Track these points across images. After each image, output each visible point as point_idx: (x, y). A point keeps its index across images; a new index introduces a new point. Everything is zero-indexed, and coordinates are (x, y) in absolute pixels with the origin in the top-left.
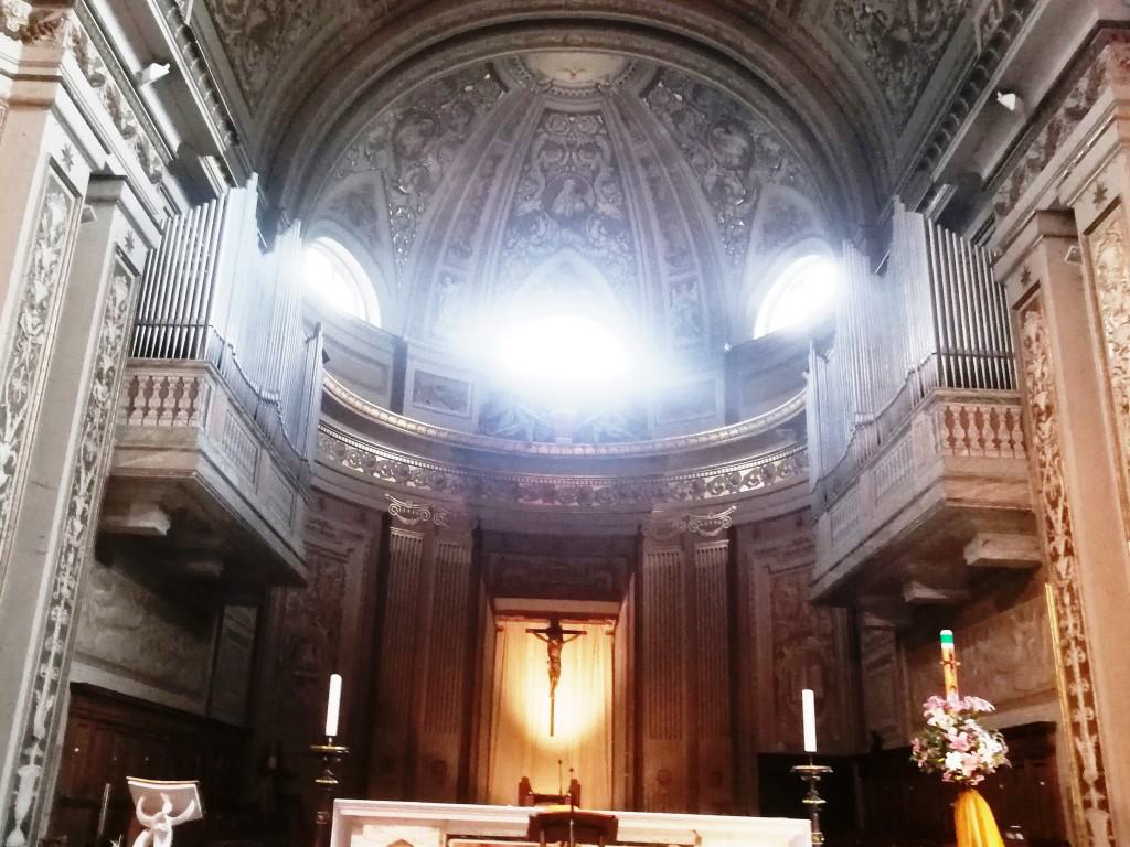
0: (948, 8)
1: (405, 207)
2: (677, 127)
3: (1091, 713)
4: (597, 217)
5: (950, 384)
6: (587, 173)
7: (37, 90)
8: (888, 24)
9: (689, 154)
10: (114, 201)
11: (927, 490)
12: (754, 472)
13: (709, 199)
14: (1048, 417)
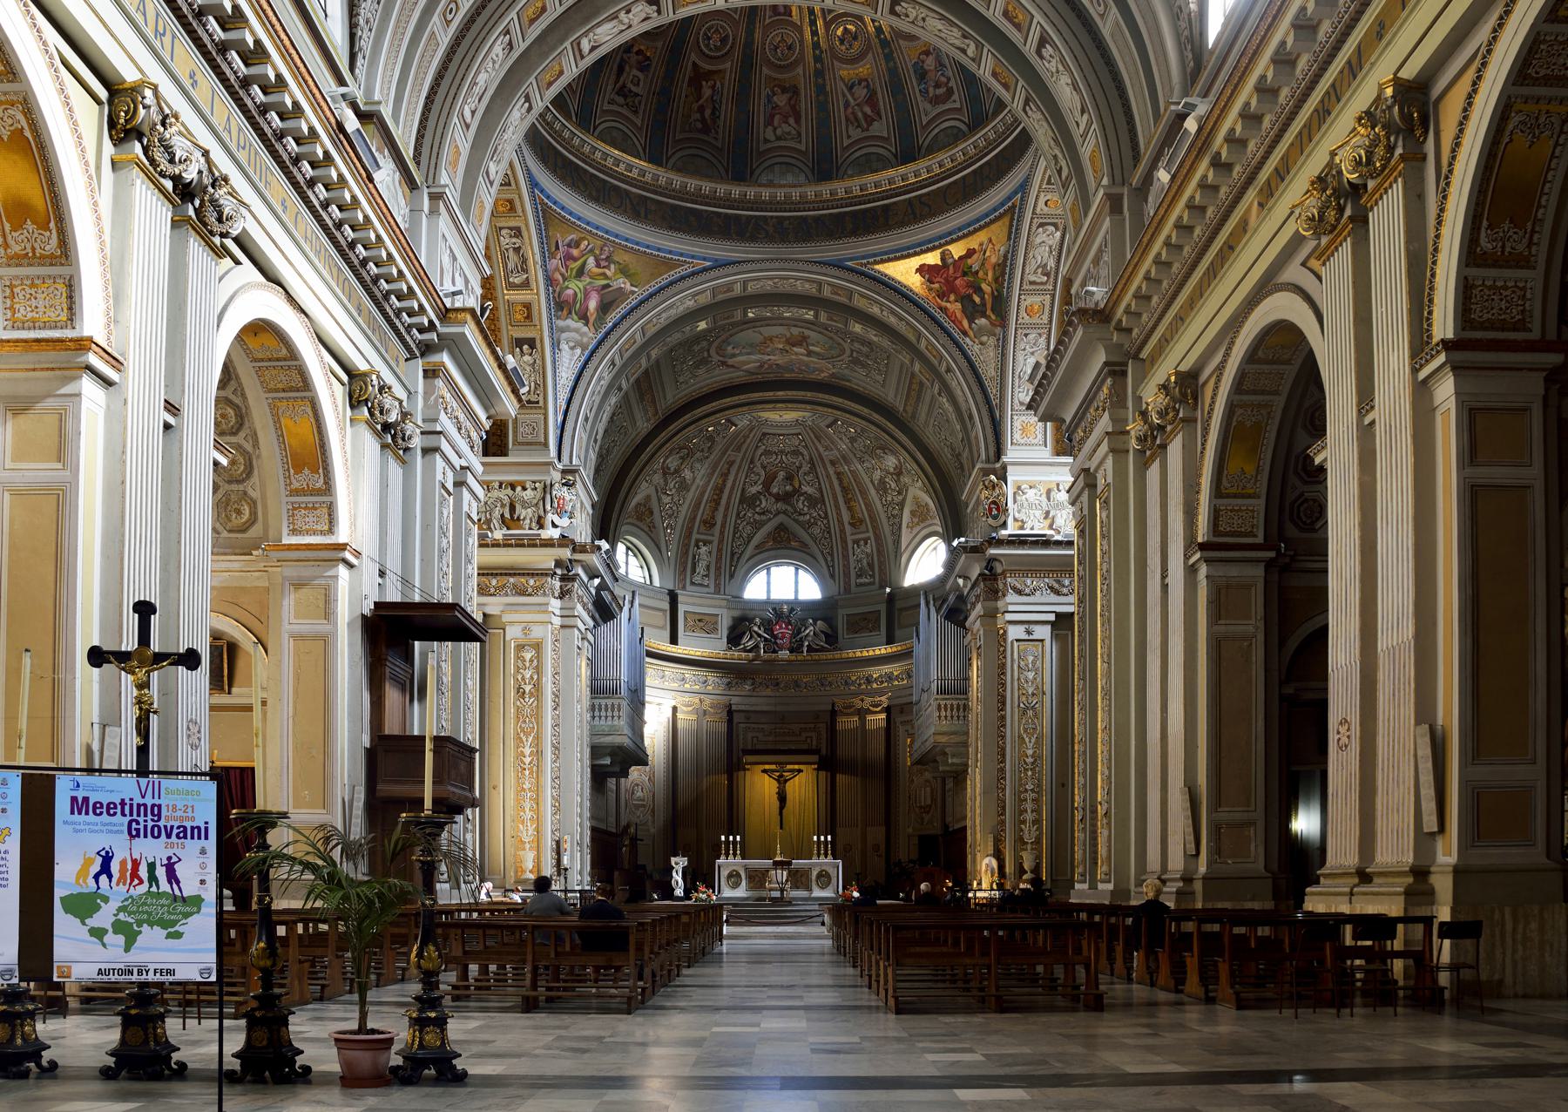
4: (802, 494)
7: (569, 621)
9: (861, 461)
10: (436, 449)
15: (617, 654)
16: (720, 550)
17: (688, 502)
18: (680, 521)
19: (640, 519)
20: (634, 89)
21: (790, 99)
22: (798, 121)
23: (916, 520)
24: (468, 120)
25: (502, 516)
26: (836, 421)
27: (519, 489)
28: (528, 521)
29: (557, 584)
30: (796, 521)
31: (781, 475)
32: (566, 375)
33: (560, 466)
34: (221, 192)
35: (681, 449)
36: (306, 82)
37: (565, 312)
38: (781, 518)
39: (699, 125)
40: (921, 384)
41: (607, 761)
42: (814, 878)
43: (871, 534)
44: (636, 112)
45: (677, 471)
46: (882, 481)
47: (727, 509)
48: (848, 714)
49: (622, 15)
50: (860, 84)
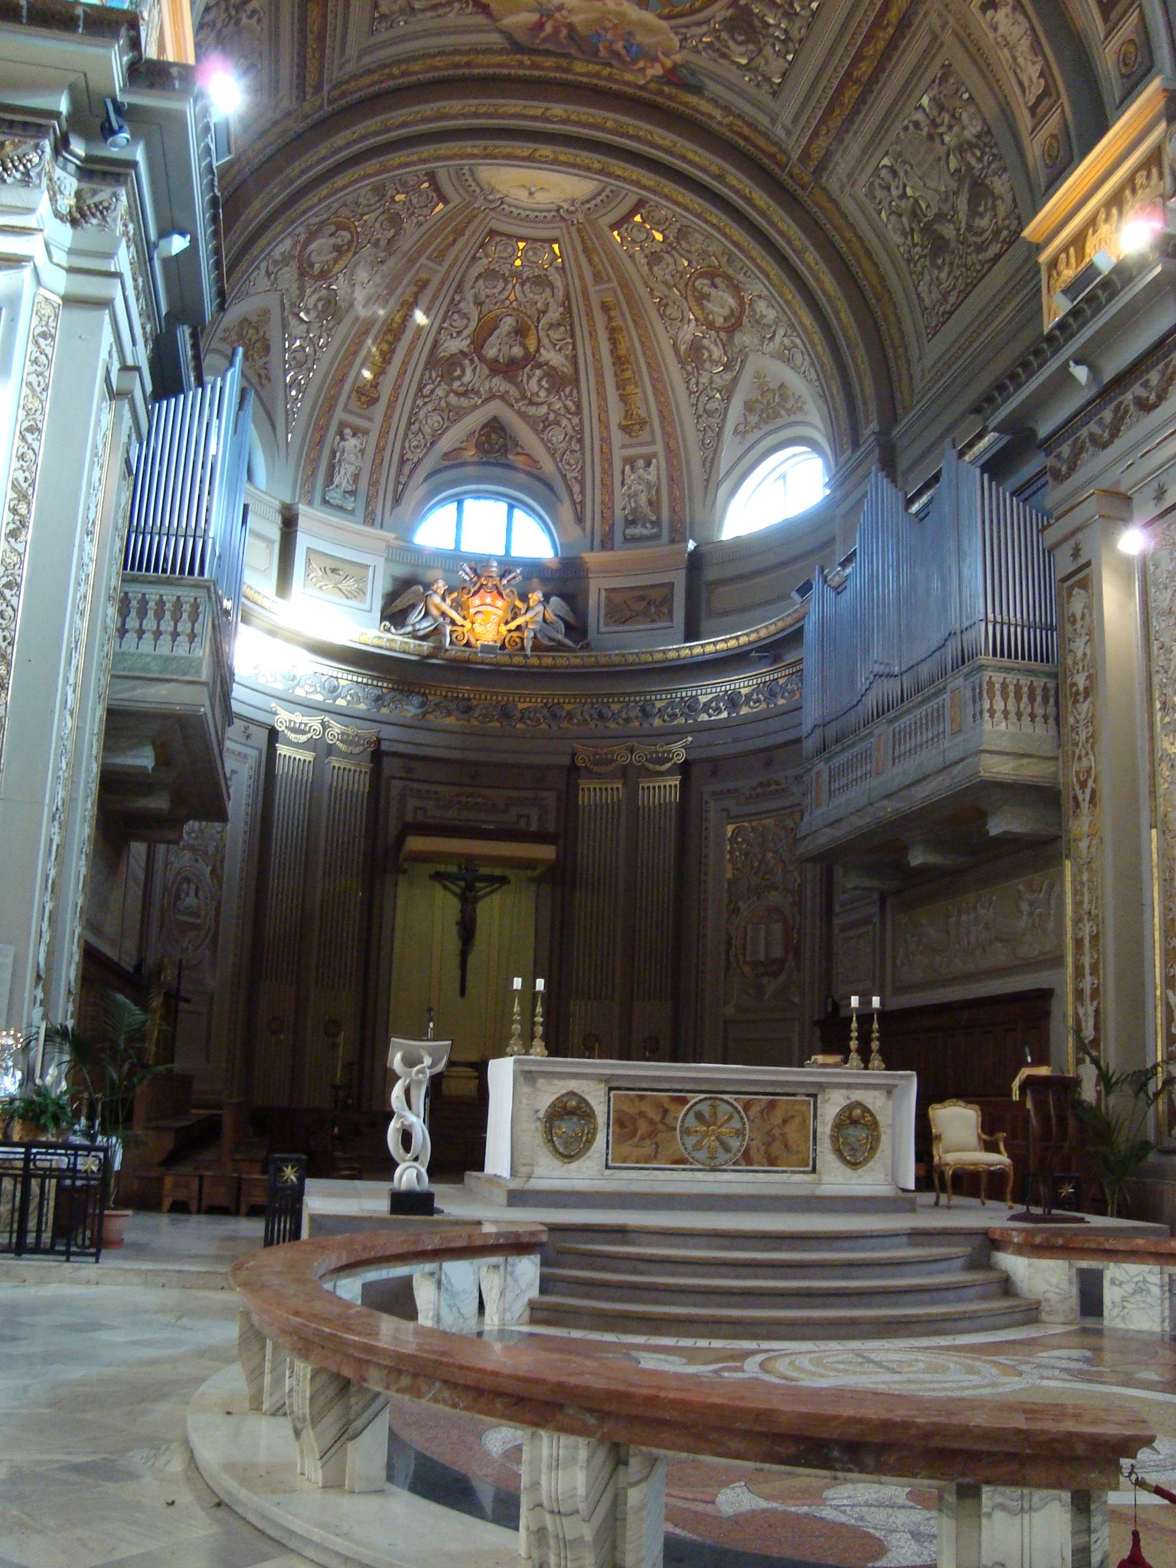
0: (1003, 220)
1: (304, 339)
2: (650, 269)
3: (1096, 981)
4: (539, 366)
5: (995, 654)
6: (532, 311)
8: (930, 215)
11: (962, 760)
13: (682, 362)
14: (1085, 698)
16: (380, 450)
23: (753, 419)
30: (522, 415)
31: (508, 323)
35: (340, 227)
38: (496, 408)
41: (144, 759)
42: (825, 1129)
43: (659, 448)
46: (696, 347)
47: (402, 374)
48: (600, 776)
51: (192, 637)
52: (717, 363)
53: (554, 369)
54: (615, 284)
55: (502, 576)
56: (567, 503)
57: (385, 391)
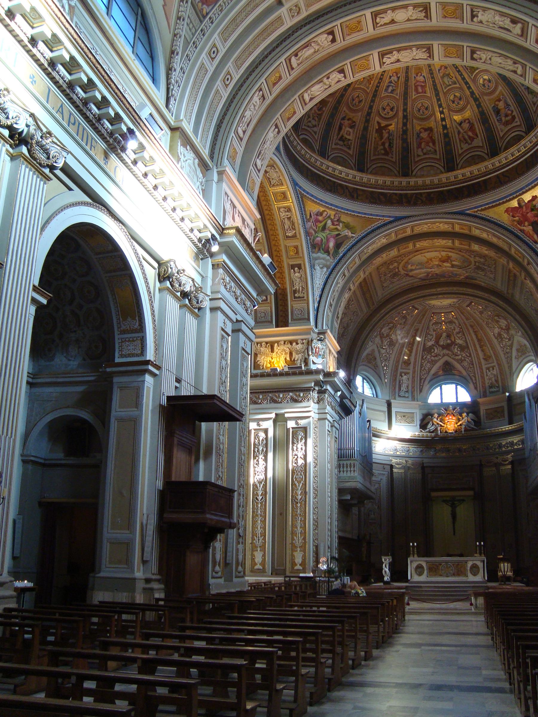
4: (456, 345)
12: (519, 441)
15: (352, 434)
16: (413, 377)
17: (395, 352)
18: (391, 362)
19: (369, 362)
20: (348, 137)
21: (429, 134)
22: (434, 144)
23: (520, 354)
24: (241, 135)
25: (286, 359)
26: (471, 302)
27: (294, 344)
28: (299, 361)
29: (315, 395)
31: (444, 335)
32: (319, 282)
33: (316, 331)
34: (48, 141)
35: (389, 324)
36: (110, 85)
37: (317, 249)
38: (446, 358)
39: (383, 152)
40: (515, 275)
41: (348, 497)
42: (469, 568)
43: (495, 364)
44: (349, 148)
45: (387, 336)
46: (499, 334)
47: (416, 355)
49: (325, 80)
50: (465, 121)
51: (354, 471)
52: (506, 338)
53: (461, 345)
54: (472, 320)
55: (454, 410)
56: (471, 383)
57: (412, 360)
